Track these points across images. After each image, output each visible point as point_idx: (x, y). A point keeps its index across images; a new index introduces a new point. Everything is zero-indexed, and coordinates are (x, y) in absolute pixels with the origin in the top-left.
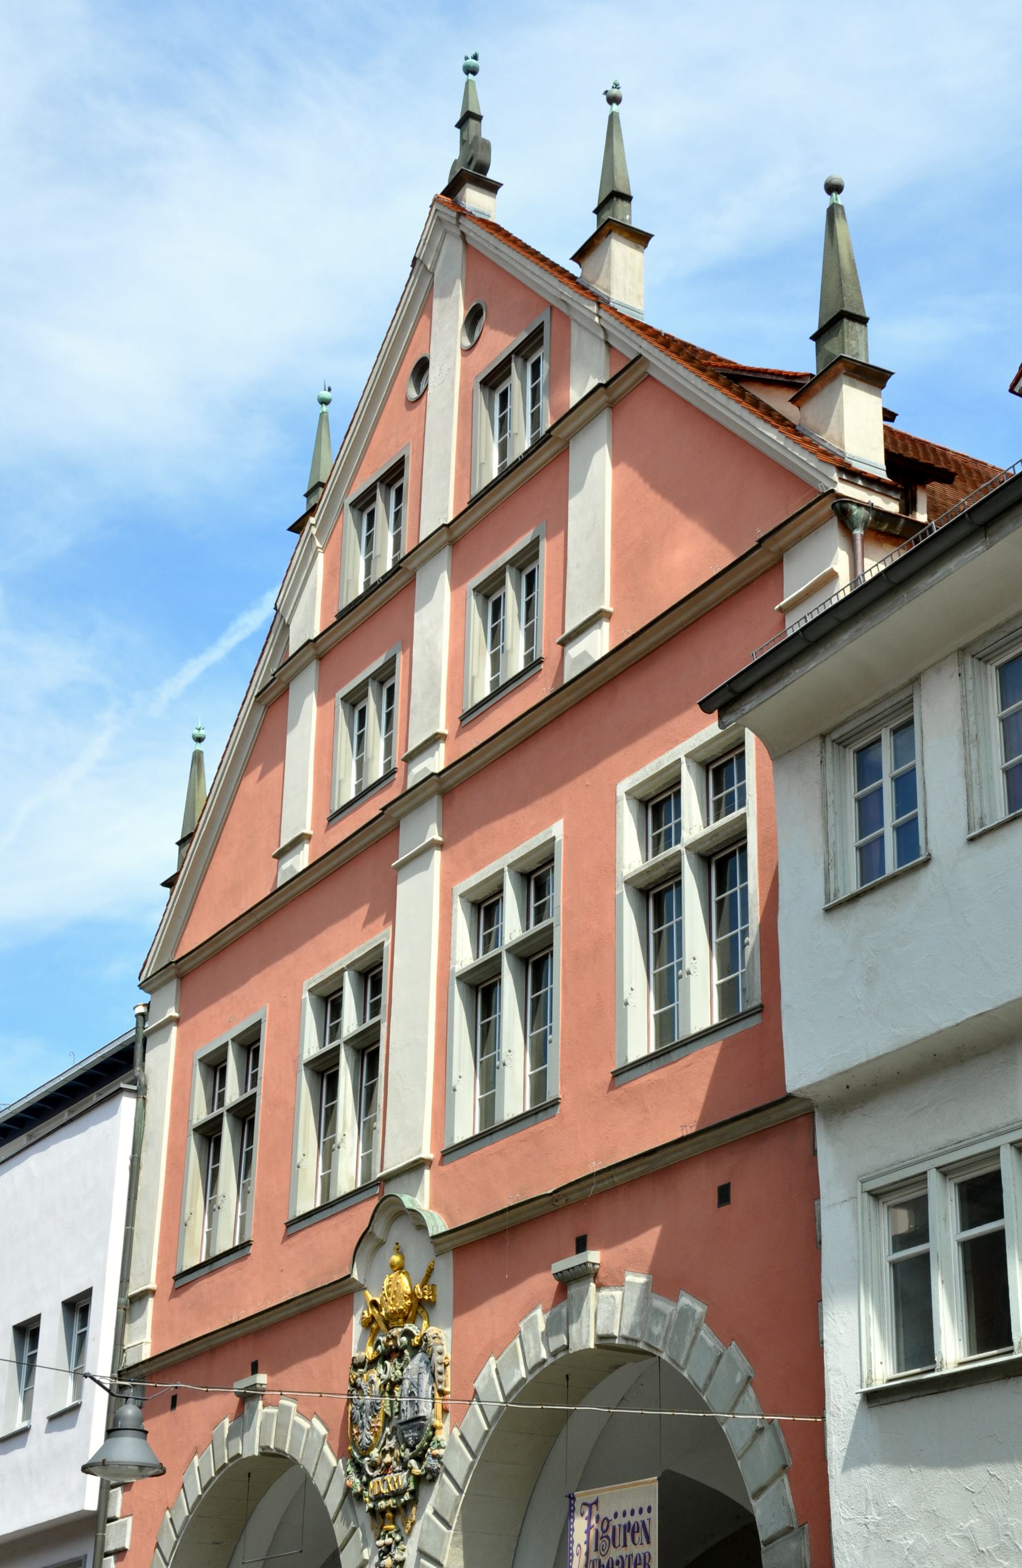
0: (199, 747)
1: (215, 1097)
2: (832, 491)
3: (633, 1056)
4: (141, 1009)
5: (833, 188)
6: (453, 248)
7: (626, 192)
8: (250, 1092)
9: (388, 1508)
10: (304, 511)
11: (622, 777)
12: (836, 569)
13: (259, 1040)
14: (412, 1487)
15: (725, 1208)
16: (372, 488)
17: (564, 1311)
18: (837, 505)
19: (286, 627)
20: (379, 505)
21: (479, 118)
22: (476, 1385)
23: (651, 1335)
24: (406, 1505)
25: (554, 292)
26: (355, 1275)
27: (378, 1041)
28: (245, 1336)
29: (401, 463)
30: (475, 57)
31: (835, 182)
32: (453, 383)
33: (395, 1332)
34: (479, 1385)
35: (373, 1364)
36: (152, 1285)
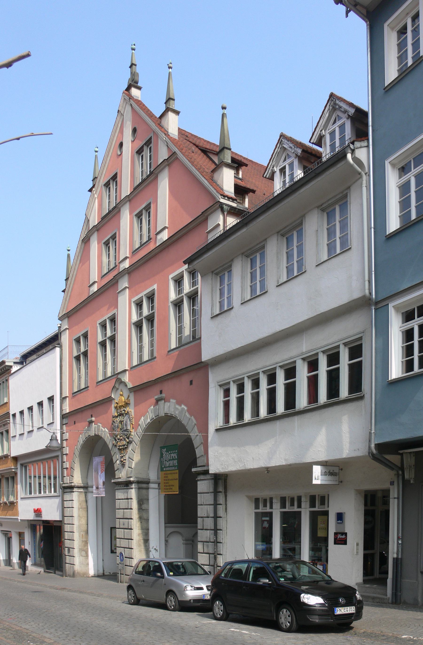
0: (69, 252)
1: (79, 350)
2: (219, 201)
3: (172, 348)
4: (59, 325)
5: (224, 108)
6: (129, 108)
7: (173, 98)
8: (87, 349)
9: (122, 448)
10: (92, 186)
11: (170, 274)
12: (220, 223)
13: (87, 336)
14: (127, 444)
15: (191, 386)
16: (109, 181)
17: (158, 407)
18: (220, 205)
19: (89, 220)
20: (111, 186)
21: (136, 65)
22: (139, 423)
23: (176, 413)
24: (126, 448)
25: (154, 128)
26: (113, 396)
27: (115, 338)
28: (89, 408)
29: (116, 174)
30: (134, 45)
31: (224, 106)
32: (129, 151)
33: (121, 410)
34: (140, 423)
35: (117, 417)
36: (68, 395)
